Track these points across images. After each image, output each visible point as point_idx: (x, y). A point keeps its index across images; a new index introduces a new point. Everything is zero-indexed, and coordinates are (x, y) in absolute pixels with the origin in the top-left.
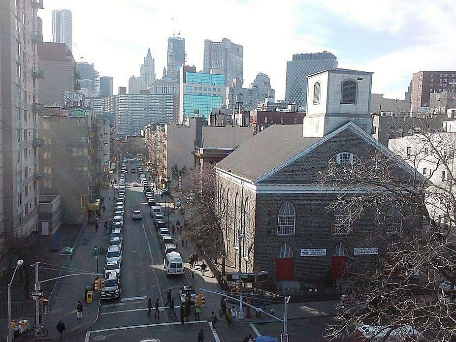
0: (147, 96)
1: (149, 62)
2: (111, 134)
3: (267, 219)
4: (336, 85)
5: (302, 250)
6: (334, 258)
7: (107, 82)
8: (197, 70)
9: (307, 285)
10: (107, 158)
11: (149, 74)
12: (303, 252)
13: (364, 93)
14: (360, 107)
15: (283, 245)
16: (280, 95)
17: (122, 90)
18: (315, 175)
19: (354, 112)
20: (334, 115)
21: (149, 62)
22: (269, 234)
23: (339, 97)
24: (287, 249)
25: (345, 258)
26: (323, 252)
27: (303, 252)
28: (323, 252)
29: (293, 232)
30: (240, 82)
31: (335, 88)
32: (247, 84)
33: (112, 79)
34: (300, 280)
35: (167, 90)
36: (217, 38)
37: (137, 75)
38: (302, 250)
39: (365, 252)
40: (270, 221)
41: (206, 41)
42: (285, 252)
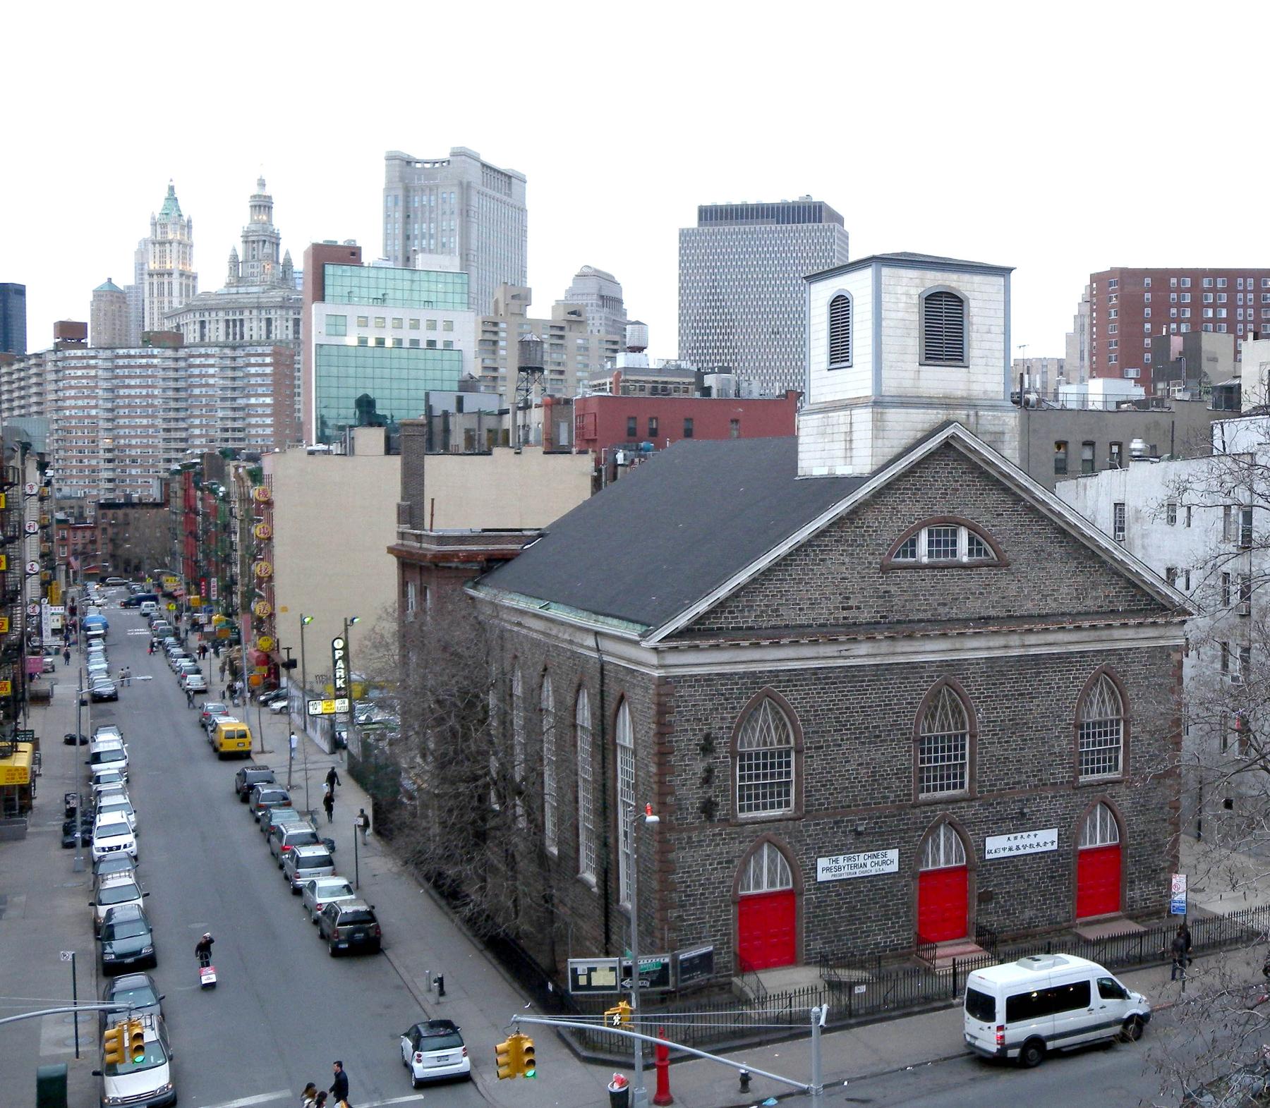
0: (169, 353)
1: (171, 229)
2: (42, 499)
3: (699, 766)
4: (901, 305)
5: (822, 863)
6: (925, 875)
7: (129, 287)
8: (366, 258)
9: (844, 975)
10: (32, 588)
11: (170, 274)
12: (827, 869)
13: (989, 332)
14: (981, 376)
15: (757, 850)
16: (663, 347)
17: (70, 333)
18: (851, 603)
19: (959, 393)
20: (906, 402)
21: (171, 229)
22: (710, 817)
23: (913, 344)
24: (772, 861)
25: (787, 898)
26: (889, 861)
27: (827, 869)
28: (889, 861)
29: (787, 804)
30: (522, 297)
31: (900, 315)
32: (541, 309)
33: (20, 291)
34: (823, 961)
35: (246, 329)
36: (429, 147)
37: (125, 279)
38: (822, 863)
39: (1018, 848)
40: (709, 771)
41: (390, 158)
42: (766, 876)
